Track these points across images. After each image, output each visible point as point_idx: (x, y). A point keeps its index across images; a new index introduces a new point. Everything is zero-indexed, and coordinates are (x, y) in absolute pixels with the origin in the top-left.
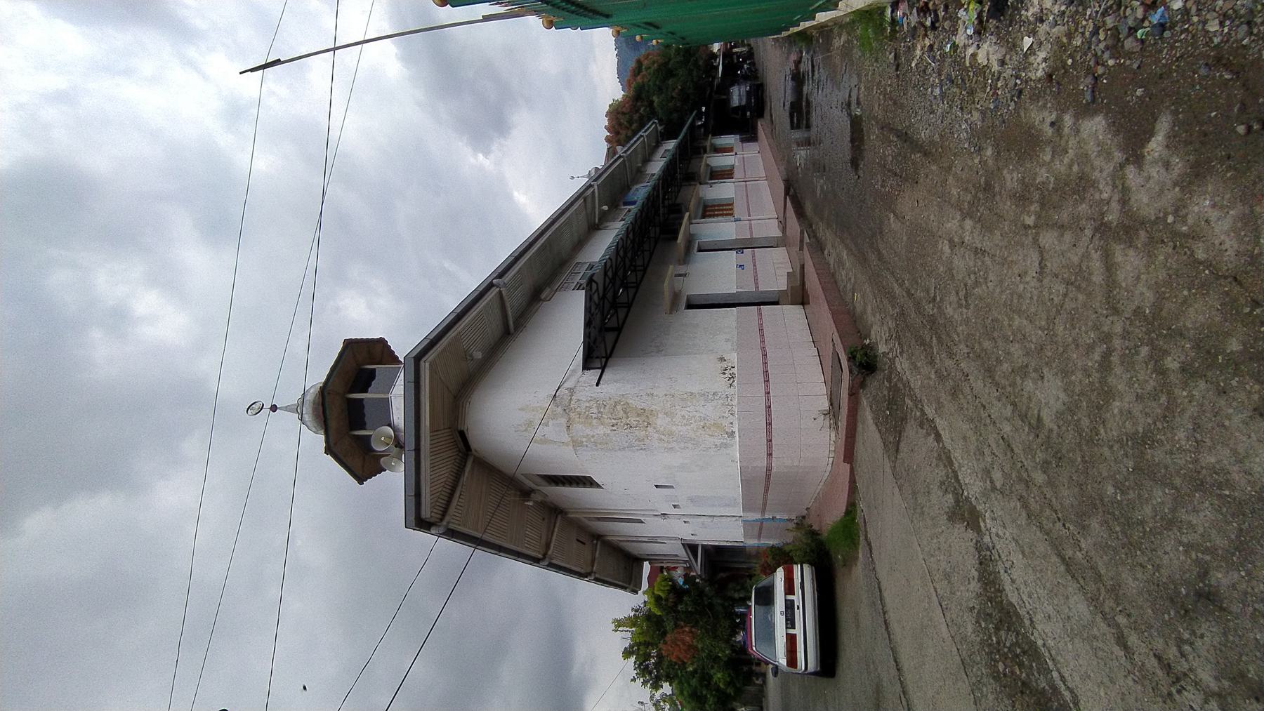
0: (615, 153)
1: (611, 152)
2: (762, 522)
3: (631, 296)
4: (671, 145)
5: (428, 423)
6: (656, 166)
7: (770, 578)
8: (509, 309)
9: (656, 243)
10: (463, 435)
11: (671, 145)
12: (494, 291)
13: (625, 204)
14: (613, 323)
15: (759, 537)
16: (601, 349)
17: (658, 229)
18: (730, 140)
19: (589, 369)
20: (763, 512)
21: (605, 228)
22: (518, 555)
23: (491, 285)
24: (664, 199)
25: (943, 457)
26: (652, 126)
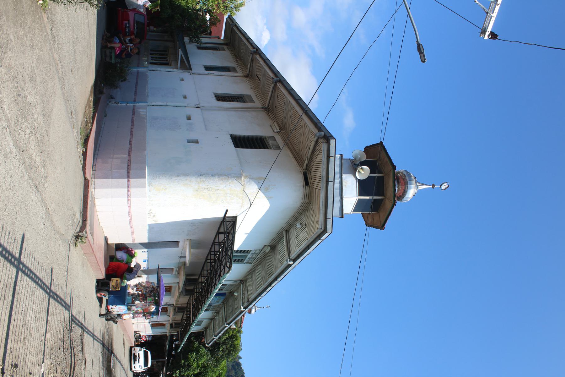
0: (236, 324)
1: (239, 324)
2: (135, 101)
3: (217, 239)
4: (194, 329)
5: (321, 196)
6: (204, 315)
7: (131, 15)
8: (285, 243)
9: (201, 274)
10: (307, 183)
11: (194, 329)
12: (293, 256)
13: (224, 294)
14: (222, 237)
15: (138, 72)
16: (227, 225)
17: (200, 280)
18: (265, 21)
19: (233, 217)
20: (134, 107)
21: (236, 281)
22: (290, 91)
23: (294, 261)
24: (190, 315)
25: (67, 345)
26: (211, 339)
